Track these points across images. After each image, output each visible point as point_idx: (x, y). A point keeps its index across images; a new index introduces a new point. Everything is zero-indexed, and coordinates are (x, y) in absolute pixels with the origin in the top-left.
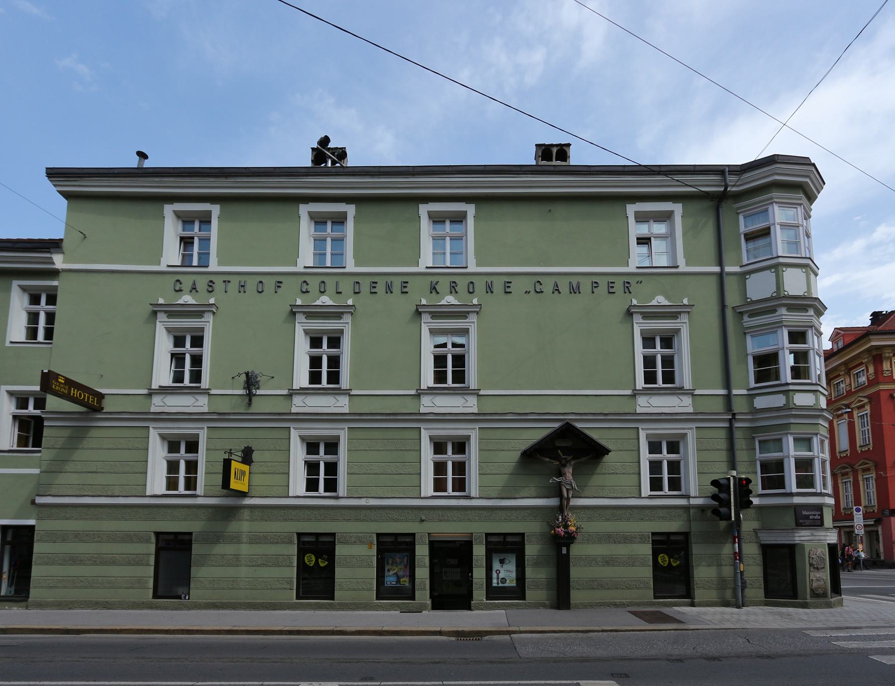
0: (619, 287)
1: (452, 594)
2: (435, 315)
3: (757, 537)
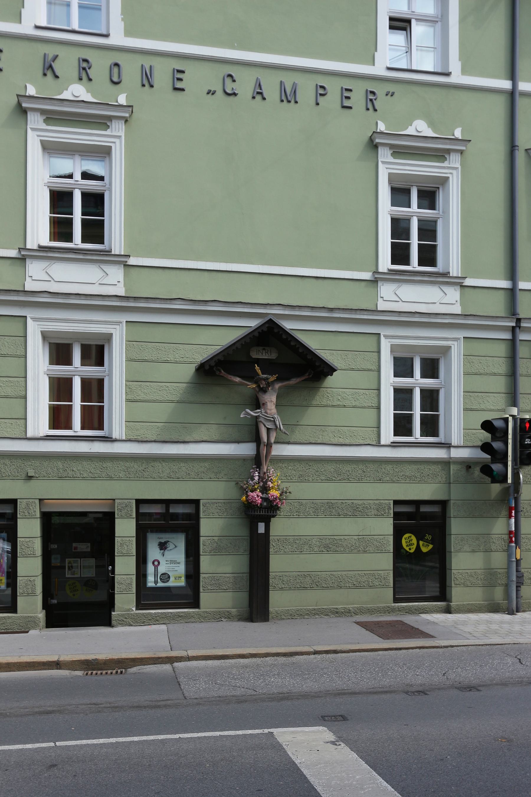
0: (358, 99)
1: (78, 603)
2: (52, 118)
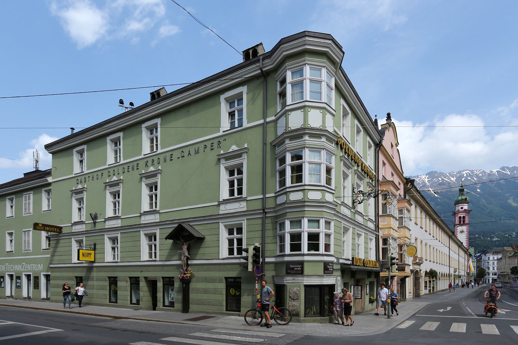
3: (274, 280)
